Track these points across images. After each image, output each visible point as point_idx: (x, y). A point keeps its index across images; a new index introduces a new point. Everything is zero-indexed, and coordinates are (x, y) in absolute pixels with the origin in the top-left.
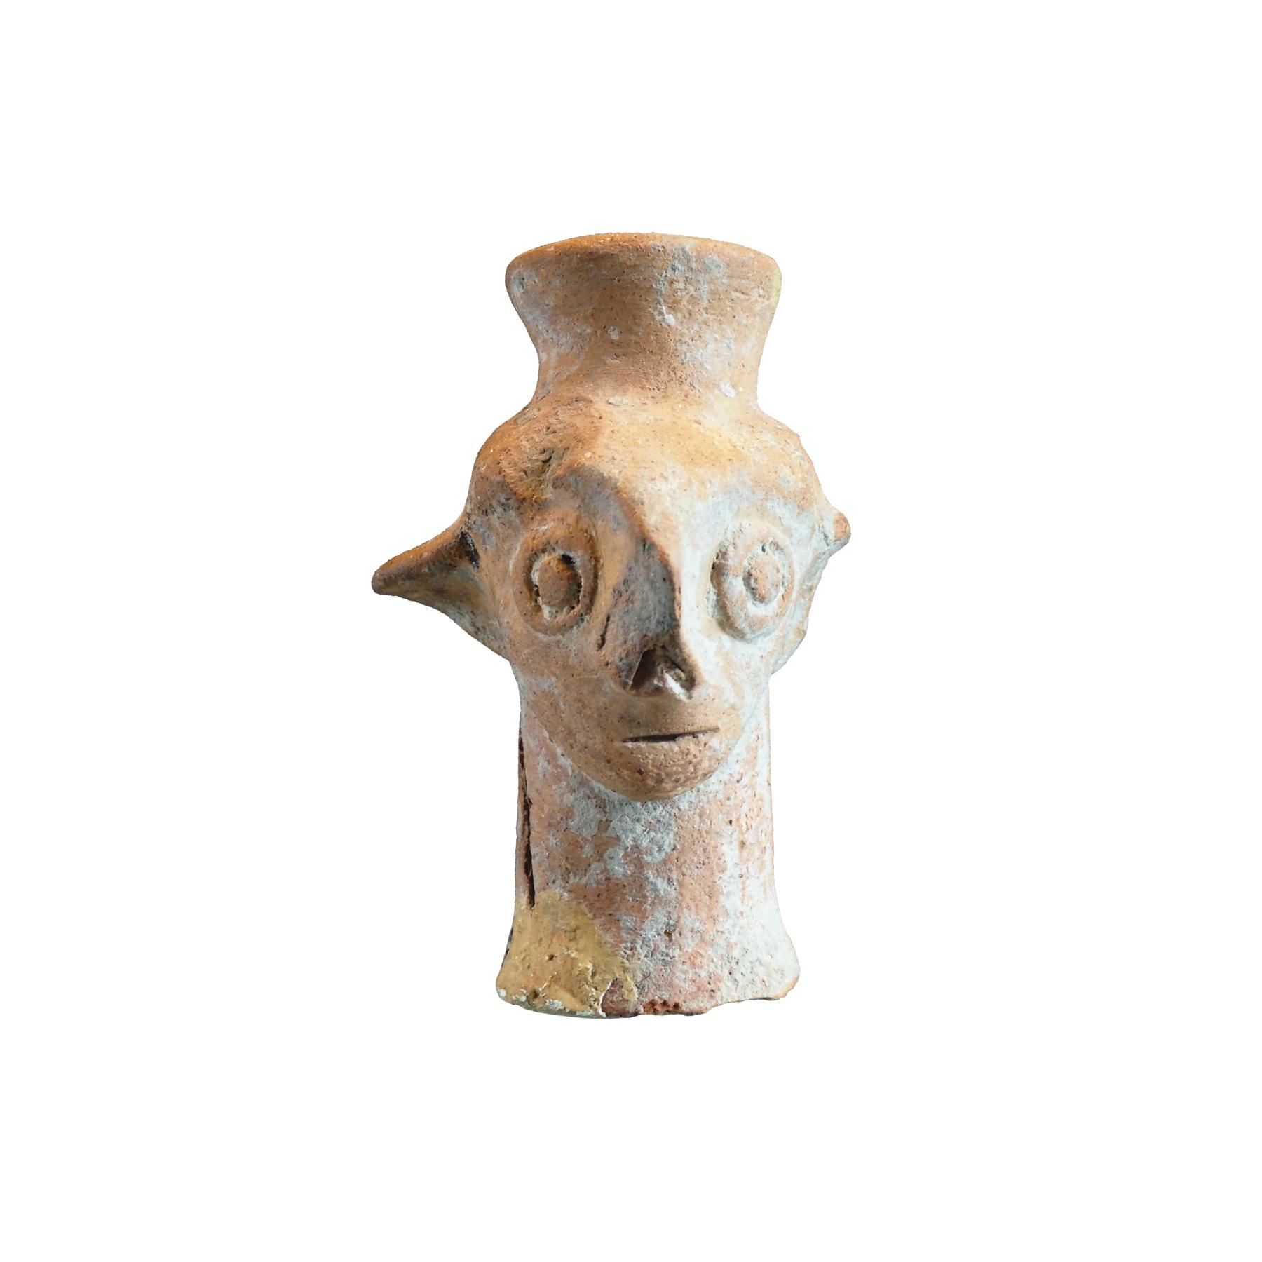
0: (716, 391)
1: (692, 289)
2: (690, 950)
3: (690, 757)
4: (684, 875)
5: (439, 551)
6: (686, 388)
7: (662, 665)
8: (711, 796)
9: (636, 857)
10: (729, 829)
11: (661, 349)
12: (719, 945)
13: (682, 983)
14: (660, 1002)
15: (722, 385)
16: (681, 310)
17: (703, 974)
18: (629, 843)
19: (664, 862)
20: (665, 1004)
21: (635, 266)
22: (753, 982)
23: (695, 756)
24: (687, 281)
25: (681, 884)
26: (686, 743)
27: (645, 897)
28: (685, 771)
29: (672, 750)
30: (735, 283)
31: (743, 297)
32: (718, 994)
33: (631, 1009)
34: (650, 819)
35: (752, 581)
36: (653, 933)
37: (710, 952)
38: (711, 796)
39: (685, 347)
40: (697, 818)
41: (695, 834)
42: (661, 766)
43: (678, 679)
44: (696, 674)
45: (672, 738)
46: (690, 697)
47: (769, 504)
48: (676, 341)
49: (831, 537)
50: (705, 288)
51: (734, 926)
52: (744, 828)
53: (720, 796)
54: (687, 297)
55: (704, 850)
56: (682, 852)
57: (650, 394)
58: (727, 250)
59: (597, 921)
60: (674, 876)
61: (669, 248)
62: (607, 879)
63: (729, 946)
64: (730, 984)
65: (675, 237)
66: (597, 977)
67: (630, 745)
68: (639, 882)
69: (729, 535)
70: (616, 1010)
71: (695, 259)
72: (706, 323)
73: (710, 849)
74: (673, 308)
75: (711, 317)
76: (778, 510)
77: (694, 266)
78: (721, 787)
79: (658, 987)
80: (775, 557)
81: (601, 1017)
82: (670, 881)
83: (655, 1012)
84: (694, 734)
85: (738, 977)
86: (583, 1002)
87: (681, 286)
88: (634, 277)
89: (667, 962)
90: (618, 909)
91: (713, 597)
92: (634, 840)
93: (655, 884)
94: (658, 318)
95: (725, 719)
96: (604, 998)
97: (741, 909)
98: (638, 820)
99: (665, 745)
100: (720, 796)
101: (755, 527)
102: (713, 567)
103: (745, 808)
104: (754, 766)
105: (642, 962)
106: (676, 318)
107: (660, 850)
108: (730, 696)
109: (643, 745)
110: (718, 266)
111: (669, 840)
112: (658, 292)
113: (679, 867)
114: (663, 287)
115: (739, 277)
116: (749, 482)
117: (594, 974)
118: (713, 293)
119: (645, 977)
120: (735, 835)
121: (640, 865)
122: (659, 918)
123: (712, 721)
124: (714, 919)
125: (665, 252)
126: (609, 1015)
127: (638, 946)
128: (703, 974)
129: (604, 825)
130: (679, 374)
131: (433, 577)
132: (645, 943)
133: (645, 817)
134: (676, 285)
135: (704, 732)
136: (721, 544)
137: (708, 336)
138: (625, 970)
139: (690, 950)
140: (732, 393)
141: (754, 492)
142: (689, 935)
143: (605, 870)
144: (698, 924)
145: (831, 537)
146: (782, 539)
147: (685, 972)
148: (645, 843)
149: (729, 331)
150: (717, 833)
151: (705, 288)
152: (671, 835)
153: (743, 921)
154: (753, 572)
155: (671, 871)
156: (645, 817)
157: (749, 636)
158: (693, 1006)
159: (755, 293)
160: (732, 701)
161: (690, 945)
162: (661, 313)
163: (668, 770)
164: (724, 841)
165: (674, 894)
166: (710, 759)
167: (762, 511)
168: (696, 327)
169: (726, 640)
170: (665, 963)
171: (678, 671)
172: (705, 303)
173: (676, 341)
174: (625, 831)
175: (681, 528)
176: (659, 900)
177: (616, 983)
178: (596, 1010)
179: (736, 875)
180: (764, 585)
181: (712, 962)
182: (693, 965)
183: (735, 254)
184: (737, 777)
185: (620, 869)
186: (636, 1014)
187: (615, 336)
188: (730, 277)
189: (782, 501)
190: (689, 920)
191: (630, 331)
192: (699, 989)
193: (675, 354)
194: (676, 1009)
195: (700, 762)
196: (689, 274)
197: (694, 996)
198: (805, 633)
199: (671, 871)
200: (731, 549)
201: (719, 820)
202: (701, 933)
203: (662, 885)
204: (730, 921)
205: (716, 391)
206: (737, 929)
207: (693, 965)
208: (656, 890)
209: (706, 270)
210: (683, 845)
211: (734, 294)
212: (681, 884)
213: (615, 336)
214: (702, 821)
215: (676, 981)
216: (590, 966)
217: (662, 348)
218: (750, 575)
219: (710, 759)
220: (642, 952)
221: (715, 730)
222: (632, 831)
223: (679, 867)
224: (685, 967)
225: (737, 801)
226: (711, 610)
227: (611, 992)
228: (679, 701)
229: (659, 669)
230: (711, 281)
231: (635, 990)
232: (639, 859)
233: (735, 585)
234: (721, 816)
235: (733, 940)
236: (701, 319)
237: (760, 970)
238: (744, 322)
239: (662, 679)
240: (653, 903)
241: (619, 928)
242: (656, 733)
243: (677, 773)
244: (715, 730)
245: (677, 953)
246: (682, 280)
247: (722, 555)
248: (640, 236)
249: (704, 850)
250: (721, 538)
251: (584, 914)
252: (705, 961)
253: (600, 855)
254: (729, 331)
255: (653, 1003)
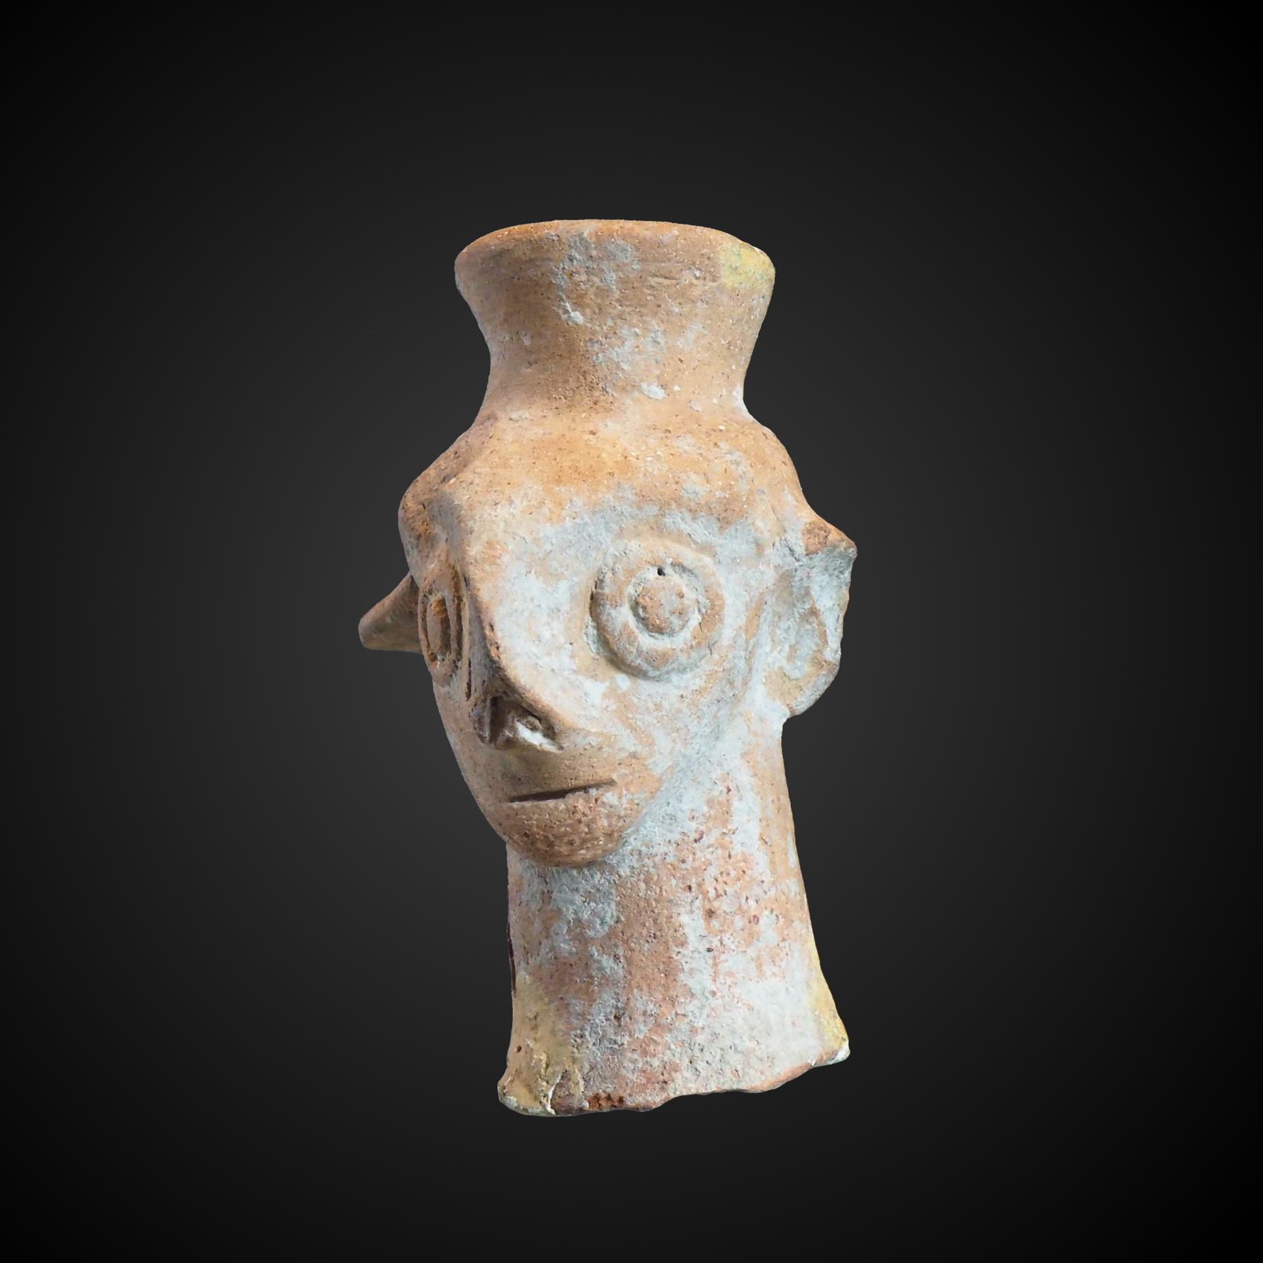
0: (636, 394)
1: (596, 279)
2: (641, 1037)
3: (578, 816)
4: (632, 950)
6: (597, 393)
7: (513, 713)
8: (657, 859)
9: (579, 932)
10: (689, 896)
11: (569, 352)
12: (679, 1030)
13: (630, 1075)
14: (603, 1095)
15: (644, 386)
16: (588, 306)
17: (656, 1063)
18: (571, 916)
19: (609, 936)
21: (531, 260)
23: (584, 815)
24: (589, 271)
25: (629, 961)
26: (579, 802)
27: (591, 977)
28: (575, 831)
29: (557, 808)
30: (652, 268)
31: (666, 282)
34: (588, 888)
35: (640, 611)
36: (602, 1017)
37: (668, 1038)
38: (657, 859)
39: (596, 347)
40: (643, 886)
41: (642, 904)
42: (548, 827)
43: (534, 729)
44: (553, 720)
45: (561, 794)
46: (561, 748)
47: (668, 520)
48: (586, 341)
49: (800, 550)
50: (612, 277)
51: (703, 1007)
52: (712, 894)
53: (670, 859)
54: (593, 290)
55: (655, 921)
56: (628, 924)
57: (555, 405)
59: (552, 1006)
60: (620, 952)
62: (556, 958)
63: (693, 1031)
64: (688, 1074)
66: (550, 1069)
67: (516, 805)
68: (586, 962)
69: (610, 562)
72: (620, 316)
73: (662, 920)
74: (579, 304)
75: (627, 310)
76: (683, 526)
77: (594, 253)
78: (672, 848)
79: (604, 1079)
80: (674, 578)
82: (616, 958)
84: (585, 788)
85: (701, 1065)
86: (536, 1098)
87: (584, 277)
88: (531, 273)
89: (616, 1050)
90: (567, 992)
91: (593, 631)
92: (576, 913)
93: (599, 962)
94: (564, 317)
95: (623, 771)
96: (554, 1092)
97: (713, 988)
98: (577, 890)
99: (551, 803)
100: (670, 859)
101: (640, 548)
102: (592, 597)
103: (713, 871)
104: (725, 823)
105: (591, 1052)
106: (584, 314)
107: (602, 923)
108: (629, 743)
109: (527, 804)
110: (624, 250)
111: (611, 911)
112: (559, 287)
113: (626, 942)
114: (561, 280)
115: (655, 260)
116: (634, 498)
117: (547, 1066)
118: (624, 282)
119: (592, 1068)
120: (697, 903)
121: (583, 940)
122: (607, 1001)
123: (602, 773)
124: (673, 1002)
125: (559, 240)
127: (587, 1034)
128: (656, 1063)
129: (547, 896)
130: (589, 378)
132: (594, 1029)
133: (584, 886)
134: (576, 278)
135: (597, 785)
136: (600, 571)
137: (624, 331)
138: (574, 1060)
139: (641, 1037)
140: (660, 393)
141: (640, 508)
142: (641, 1019)
143: (552, 949)
144: (651, 1006)
145: (800, 550)
146: (689, 556)
147: (634, 1062)
148: (586, 916)
149: (654, 323)
150: (670, 901)
151: (612, 277)
152: (613, 906)
153: (714, 1002)
154: (641, 600)
155: (616, 946)
156: (584, 886)
157: (651, 673)
159: (687, 278)
160: (632, 749)
161: (642, 1030)
162: (566, 312)
163: (555, 831)
164: (682, 910)
165: (621, 972)
166: (608, 816)
167: (658, 528)
168: (610, 323)
169: (623, 681)
170: (614, 1052)
171: (531, 719)
172: (617, 295)
173: (586, 341)
174: (566, 901)
175: (506, 558)
176: (607, 981)
177: (566, 1076)
179: (702, 949)
180: (663, 614)
182: (645, 1053)
184: (694, 836)
185: (566, 947)
187: (527, 342)
188: (641, 261)
189: (688, 516)
190: (641, 1001)
191: (540, 335)
192: (649, 1080)
193: (585, 356)
195: (593, 821)
196: (589, 263)
199: (616, 946)
200: (609, 575)
201: (672, 885)
202: (656, 1017)
203: (607, 962)
204: (696, 1002)
205: (636, 394)
206: (706, 1011)
207: (645, 1053)
208: (601, 969)
209: (610, 256)
210: (628, 918)
211: (653, 281)
212: (629, 961)
213: (527, 342)
214: (648, 888)
215: (624, 1072)
216: (544, 1057)
217: (572, 350)
218: (637, 603)
219: (608, 816)
220: (591, 1040)
221: (611, 783)
222: (572, 903)
223: (626, 942)
224: (635, 1056)
225: (697, 864)
226: (593, 647)
227: (560, 1085)
228: (555, 755)
229: (510, 717)
230: (618, 268)
231: (582, 1082)
232: (581, 934)
233: (622, 617)
234: (674, 882)
235: (699, 1023)
236: (614, 312)
238: (676, 310)
239: (513, 729)
240: (600, 985)
241: (570, 1013)
242: (539, 790)
243: (566, 834)
244: (611, 783)
245: (626, 1039)
246: (582, 270)
247: (599, 583)
249: (655, 921)
250: (600, 563)
251: (542, 999)
252: (660, 1048)
253: (547, 931)
254: (654, 322)
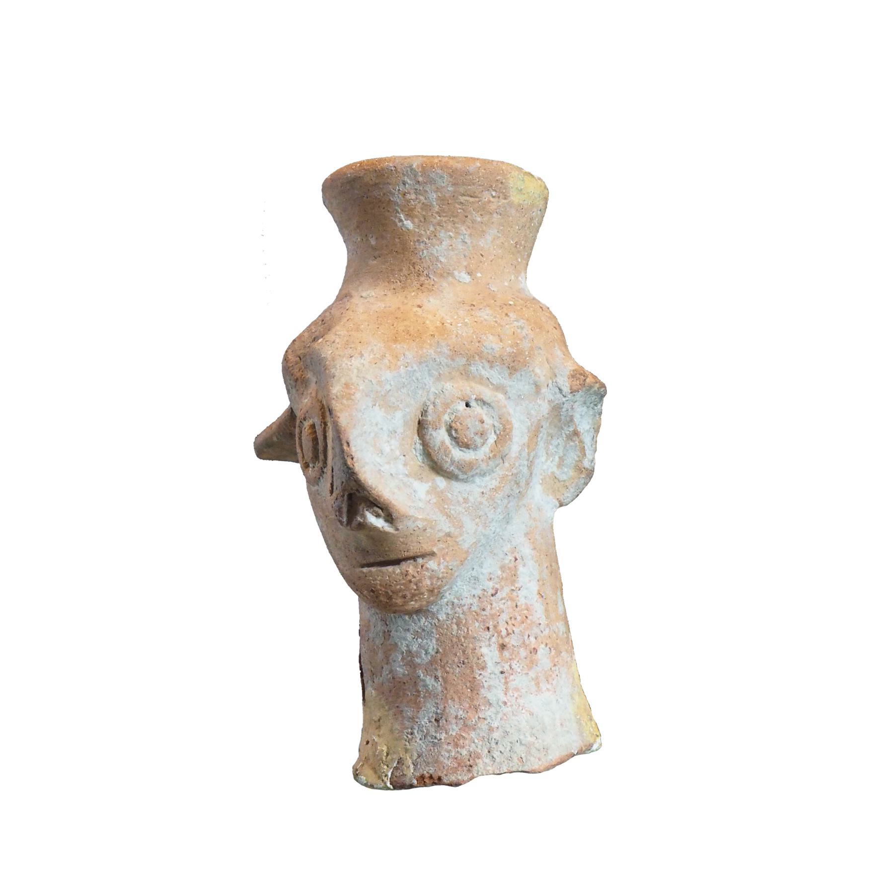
0: (450, 279)
1: (422, 198)
2: (454, 734)
3: (409, 578)
4: (448, 673)
5: (280, 424)
6: (422, 279)
7: (363, 505)
8: (465, 608)
9: (410, 660)
10: (488, 634)
11: (403, 249)
12: (480, 729)
13: (446, 761)
14: (427, 775)
15: (456, 273)
16: (416, 216)
17: (464, 752)
18: (404, 649)
19: (431, 663)
20: (431, 777)
21: (376, 184)
22: (510, 759)
23: (414, 577)
24: (417, 192)
25: (445, 680)
26: (410, 567)
27: (418, 692)
28: (407, 588)
29: (394, 572)
30: (462, 190)
31: (471, 199)
32: (475, 769)
33: (408, 782)
34: (416, 628)
35: (453, 432)
36: (426, 720)
37: (473, 734)
38: (465, 608)
39: (422, 246)
40: (455, 627)
41: (455, 640)
42: (388, 586)
43: (378, 516)
44: (391, 510)
45: (397, 562)
46: (397, 529)
48: (414, 242)
49: (566, 389)
50: (433, 196)
51: (498, 713)
52: (504, 633)
53: (474, 608)
54: (420, 205)
55: (464, 652)
56: (445, 654)
57: (393, 286)
58: (451, 162)
59: (391, 712)
60: (439, 674)
61: (399, 167)
62: (393, 678)
63: (491, 729)
64: (487, 761)
65: (405, 158)
66: (389, 757)
67: (365, 570)
68: (415, 681)
69: (432, 398)
70: (399, 785)
71: (426, 171)
72: (439, 224)
73: (469, 651)
74: (410, 215)
75: (444, 219)
76: (483, 372)
77: (420, 179)
78: (475, 600)
79: (428, 764)
80: (477, 409)
81: (389, 789)
82: (436, 678)
83: (425, 785)
84: (414, 558)
85: (496, 754)
86: (379, 777)
87: (413, 196)
88: (376, 193)
89: (436, 744)
90: (401, 702)
91: (419, 447)
92: (407, 646)
93: (424, 681)
94: (399, 224)
95: (441, 545)
96: (392, 773)
97: (505, 699)
98: (408, 630)
99: (390, 569)
100: (474, 608)
101: (453, 388)
102: (419, 423)
103: (505, 616)
104: (513, 582)
105: (418, 744)
106: (413, 223)
107: (426, 653)
108: (445, 526)
109: (373, 569)
110: (441, 177)
111: (432, 645)
112: (396, 203)
113: (443, 667)
114: (397, 199)
115: (464, 184)
116: (449, 352)
117: (388, 755)
118: (442, 200)
119: (419, 756)
120: (494, 639)
121: (412, 665)
122: (430, 709)
123: (426, 547)
124: (476, 709)
125: (396, 170)
126: (395, 788)
127: (415, 732)
128: (464, 752)
129: (387, 635)
130: (417, 268)
131: (275, 444)
132: (420, 728)
133: (413, 627)
134: (408, 196)
135: (423, 556)
136: (425, 404)
137: (442, 235)
138: (407, 750)
139: (454, 734)
140: (467, 278)
141: (453, 360)
142: (454, 721)
143: (391, 671)
144: (461, 712)
145: (566, 389)
146: (487, 394)
147: (449, 751)
148: (414, 648)
149: (463, 229)
150: (474, 638)
151: (433, 196)
152: (434, 641)
153: (506, 709)
154: (454, 425)
155: (436, 670)
156: (413, 627)
157: (461, 477)
158: (453, 778)
159: (486, 197)
160: (448, 530)
161: (454, 729)
162: (401, 221)
163: (393, 588)
164: (483, 644)
165: (440, 688)
166: (431, 578)
167: (466, 374)
168: (432, 228)
169: (441, 482)
170: (434, 744)
171: (376, 509)
172: (437, 208)
173: (414, 242)
174: (401, 638)
175: (358, 395)
176: (430, 694)
177: (400, 761)
178: (385, 783)
179: (497, 672)
180: (469, 435)
181: (474, 742)
182: (456, 745)
183: (459, 166)
184: (491, 591)
185: (401, 670)
186: (411, 786)
187: (373, 242)
188: (454, 184)
189: (487, 365)
190: (454, 709)
191: (382, 237)
192: (459, 764)
193: (414, 252)
194: (439, 781)
195: (420, 581)
196: (417, 186)
197: (455, 770)
198: (590, 474)
199: (436, 670)
200: (431, 407)
201: (476, 627)
202: (464, 720)
203: (430, 681)
204: (492, 709)
205: (450, 279)
206: (500, 716)
207: (456, 745)
208: (426, 686)
209: (432, 182)
210: (444, 650)
211: (462, 199)
212: (445, 680)
213: (373, 242)
214: (459, 628)
215: (442, 759)
216: (385, 748)
217: (405, 248)
218: (451, 427)
219: (431, 578)
220: (418, 736)
221: (432, 554)
222: (405, 639)
223: (443, 667)
224: (450, 748)
225: (493, 611)
226: (420, 458)
227: (396, 768)
228: (393, 534)
229: (361, 508)
230: (438, 190)
231: (412, 766)
232: (412, 661)
233: (440, 436)
234: (477, 624)
235: (495, 724)
236: (435, 221)
237: (520, 750)
238: (479, 219)
239: (363, 516)
240: (425, 697)
241: (403, 717)
242: (381, 559)
243: (400, 590)
244: (432, 554)
245: (443, 736)
246: (412, 191)
247: (424, 413)
248: (380, 160)
249: (464, 652)
250: (424, 399)
251: (383, 707)
252: (467, 742)
253: (387, 659)
254: (463, 228)
255: (422, 777)
